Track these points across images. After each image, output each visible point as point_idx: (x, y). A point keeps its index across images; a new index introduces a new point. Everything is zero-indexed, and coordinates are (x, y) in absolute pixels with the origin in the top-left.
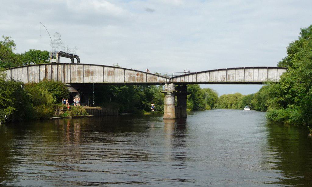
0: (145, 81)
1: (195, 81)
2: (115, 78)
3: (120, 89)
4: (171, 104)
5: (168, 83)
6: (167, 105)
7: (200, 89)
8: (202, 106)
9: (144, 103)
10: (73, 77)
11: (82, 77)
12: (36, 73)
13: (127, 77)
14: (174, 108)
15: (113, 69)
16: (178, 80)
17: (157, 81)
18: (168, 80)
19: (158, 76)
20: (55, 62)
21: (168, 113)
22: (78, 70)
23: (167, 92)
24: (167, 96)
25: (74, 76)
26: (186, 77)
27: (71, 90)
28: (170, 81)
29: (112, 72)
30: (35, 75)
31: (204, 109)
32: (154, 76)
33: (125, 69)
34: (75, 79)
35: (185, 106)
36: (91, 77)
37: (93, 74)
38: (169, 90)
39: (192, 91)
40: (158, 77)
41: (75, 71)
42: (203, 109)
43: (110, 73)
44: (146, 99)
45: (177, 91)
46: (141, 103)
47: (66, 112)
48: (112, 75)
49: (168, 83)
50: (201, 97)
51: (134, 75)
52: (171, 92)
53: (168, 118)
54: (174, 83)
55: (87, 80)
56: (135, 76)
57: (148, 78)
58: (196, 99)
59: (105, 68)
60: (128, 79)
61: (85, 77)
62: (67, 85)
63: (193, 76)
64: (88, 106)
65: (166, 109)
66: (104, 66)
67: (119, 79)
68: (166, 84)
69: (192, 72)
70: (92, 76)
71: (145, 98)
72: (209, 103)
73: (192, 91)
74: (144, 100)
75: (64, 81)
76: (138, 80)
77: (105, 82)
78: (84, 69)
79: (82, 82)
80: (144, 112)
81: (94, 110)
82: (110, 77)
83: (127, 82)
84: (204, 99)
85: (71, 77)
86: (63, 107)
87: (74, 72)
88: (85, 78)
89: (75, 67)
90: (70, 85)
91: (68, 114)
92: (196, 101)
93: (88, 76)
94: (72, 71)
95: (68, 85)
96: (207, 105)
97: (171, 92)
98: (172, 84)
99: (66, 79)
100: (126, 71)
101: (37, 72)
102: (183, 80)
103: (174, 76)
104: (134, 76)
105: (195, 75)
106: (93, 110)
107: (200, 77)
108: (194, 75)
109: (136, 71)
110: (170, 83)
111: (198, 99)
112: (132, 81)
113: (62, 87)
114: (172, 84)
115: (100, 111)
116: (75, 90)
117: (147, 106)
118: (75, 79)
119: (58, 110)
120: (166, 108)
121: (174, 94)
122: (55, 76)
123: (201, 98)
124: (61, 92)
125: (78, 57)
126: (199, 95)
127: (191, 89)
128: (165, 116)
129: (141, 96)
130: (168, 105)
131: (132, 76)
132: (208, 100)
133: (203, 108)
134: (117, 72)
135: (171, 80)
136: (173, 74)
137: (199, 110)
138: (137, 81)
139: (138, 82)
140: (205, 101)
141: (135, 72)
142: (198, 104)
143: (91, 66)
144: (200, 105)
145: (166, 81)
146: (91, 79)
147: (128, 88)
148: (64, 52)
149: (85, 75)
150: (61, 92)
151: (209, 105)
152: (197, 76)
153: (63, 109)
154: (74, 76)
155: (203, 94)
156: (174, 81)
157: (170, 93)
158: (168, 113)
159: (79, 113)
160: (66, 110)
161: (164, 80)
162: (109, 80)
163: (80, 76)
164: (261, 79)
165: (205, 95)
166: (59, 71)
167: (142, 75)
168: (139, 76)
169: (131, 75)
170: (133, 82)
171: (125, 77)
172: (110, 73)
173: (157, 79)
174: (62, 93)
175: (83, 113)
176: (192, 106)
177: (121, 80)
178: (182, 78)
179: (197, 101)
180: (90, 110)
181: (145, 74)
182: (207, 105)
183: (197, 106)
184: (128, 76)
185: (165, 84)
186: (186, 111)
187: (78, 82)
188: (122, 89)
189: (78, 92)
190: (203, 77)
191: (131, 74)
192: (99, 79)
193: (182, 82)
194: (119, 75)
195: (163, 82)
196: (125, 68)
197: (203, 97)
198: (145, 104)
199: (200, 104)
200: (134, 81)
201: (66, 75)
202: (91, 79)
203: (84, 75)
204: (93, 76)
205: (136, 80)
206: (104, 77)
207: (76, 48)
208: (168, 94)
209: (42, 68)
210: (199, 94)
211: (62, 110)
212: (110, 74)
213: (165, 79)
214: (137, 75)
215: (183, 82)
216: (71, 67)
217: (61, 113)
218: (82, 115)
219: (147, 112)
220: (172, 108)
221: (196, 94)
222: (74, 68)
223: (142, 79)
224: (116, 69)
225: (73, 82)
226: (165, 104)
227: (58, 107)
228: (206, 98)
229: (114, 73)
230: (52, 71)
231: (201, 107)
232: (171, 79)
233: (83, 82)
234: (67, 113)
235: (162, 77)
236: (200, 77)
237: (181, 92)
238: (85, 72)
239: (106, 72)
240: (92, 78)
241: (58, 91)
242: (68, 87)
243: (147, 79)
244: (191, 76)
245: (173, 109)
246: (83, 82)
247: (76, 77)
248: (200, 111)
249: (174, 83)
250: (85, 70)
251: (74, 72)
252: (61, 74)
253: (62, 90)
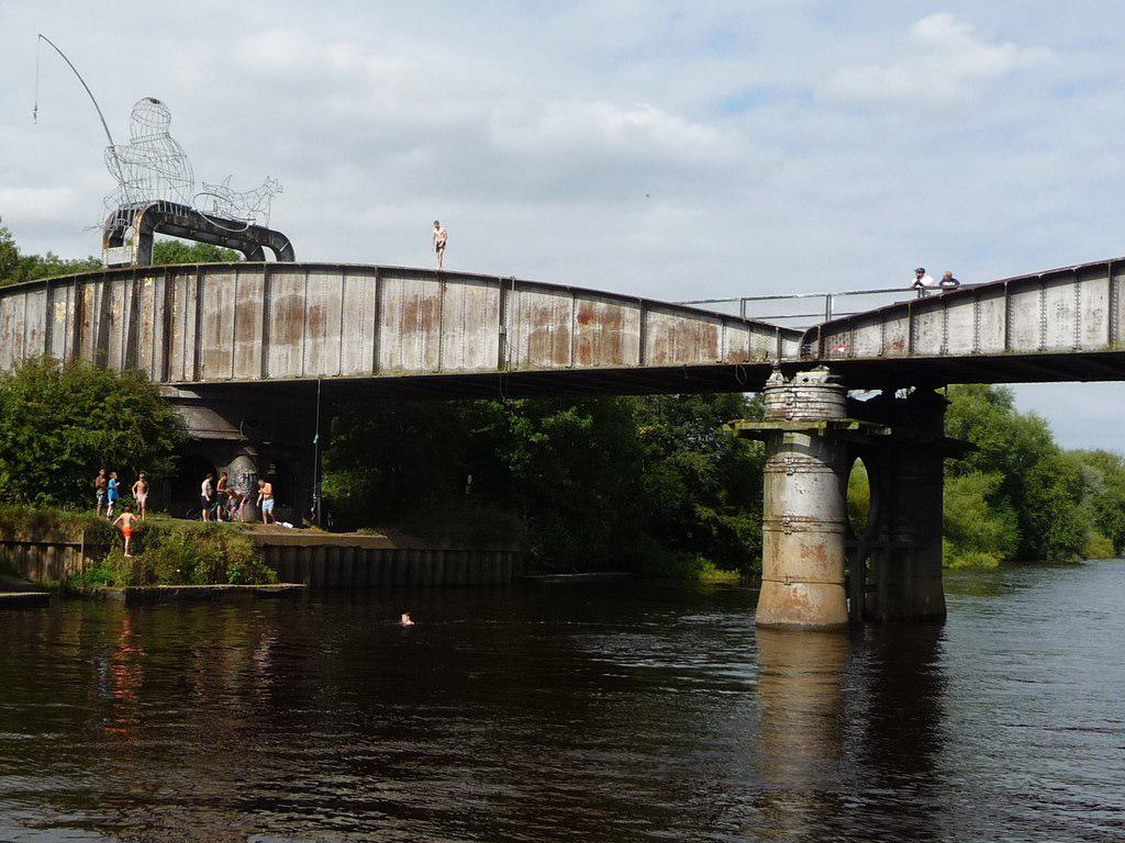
0: (631, 360)
1: (993, 344)
2: (447, 344)
3: (538, 428)
4: (809, 520)
5: (789, 370)
6: (784, 525)
7: (1055, 451)
8: (1066, 538)
9: (705, 512)
10: (213, 348)
11: (258, 342)
12: (33, 333)
13: (520, 335)
14: (834, 550)
15: (431, 288)
16: (869, 343)
17: (713, 355)
18: (792, 349)
19: (726, 320)
20: (125, 264)
21: (789, 581)
22: (242, 301)
23: (780, 433)
24: (785, 456)
25: (218, 342)
26: (922, 318)
27: (196, 423)
28: (804, 352)
29: (427, 304)
30: (29, 341)
31: (1076, 558)
32: (696, 324)
33: (506, 285)
34: (223, 358)
35: (933, 526)
36: (309, 341)
37: (321, 328)
38: (798, 412)
39: (1011, 458)
40: (719, 328)
41: (227, 308)
42: (1071, 554)
43: (419, 317)
44: (722, 495)
45: (855, 426)
46: (691, 513)
47: (108, 560)
48: (426, 324)
49: (789, 370)
50: (1058, 489)
51: (563, 319)
52: (811, 432)
53: (785, 621)
54: (835, 367)
55: (284, 364)
56: (569, 325)
57: (651, 339)
58: (1030, 501)
59: (393, 286)
60: (524, 352)
61: (279, 342)
62: (176, 393)
63: (977, 311)
64: (314, 523)
65: (776, 553)
66: (383, 273)
67: (472, 352)
68: (775, 378)
69: (969, 278)
70: (315, 335)
71: (715, 490)
72: (1103, 525)
73: (1011, 458)
74: (710, 501)
75: (167, 369)
76: (585, 350)
77: (388, 369)
78: (274, 299)
79: (255, 377)
80: (701, 568)
81: (336, 553)
82: (418, 343)
83: (520, 369)
84: (1077, 500)
85: (204, 346)
86: (81, 527)
87: (219, 317)
88: (275, 351)
89: (225, 285)
90: (195, 396)
91: (119, 569)
92: (1034, 515)
93: (292, 337)
94: (209, 309)
95: (183, 394)
96: (1094, 536)
97: (811, 432)
98: (819, 375)
99: (177, 360)
100: (515, 298)
101: (39, 326)
102: (899, 345)
103: (834, 318)
104: (562, 329)
105: (998, 304)
106: (328, 549)
107: (1036, 311)
108: (984, 305)
109: (576, 293)
110: (807, 367)
111: (1043, 502)
112: (547, 363)
113: (129, 403)
114: (819, 375)
115: (377, 557)
116: (224, 425)
117: (727, 532)
118: (223, 358)
119: (60, 547)
120: (776, 545)
121: (834, 446)
122: (150, 354)
123: (1058, 497)
124: (115, 435)
125: (286, 240)
126: (1047, 482)
127: (1005, 452)
128: (769, 606)
129: (689, 476)
130: (787, 525)
131: (552, 327)
132: (1100, 509)
133: (1073, 550)
134: (459, 303)
135: (815, 347)
136: (828, 304)
137: (1049, 557)
138: (583, 360)
139: (591, 366)
140: (1083, 513)
141: (571, 300)
142: (1046, 527)
143: (313, 277)
144: (1056, 535)
145: (780, 354)
146: (307, 358)
147: (587, 422)
148: (186, 210)
149: (279, 330)
150: (115, 435)
151: (1107, 535)
152: (1016, 309)
153: (81, 540)
154: (218, 342)
155: (1071, 478)
156: (839, 349)
157: (803, 440)
158: (789, 581)
159: (201, 569)
160: (107, 549)
161: (761, 347)
162: (408, 357)
163: (249, 337)
164: (954, 590)
165: (1081, 481)
166: (143, 317)
167: (616, 319)
168: (598, 327)
169: (541, 323)
170: (556, 366)
171: (502, 336)
172: (419, 317)
173: (712, 344)
174: (121, 440)
175: (232, 571)
176: (1011, 537)
177: (483, 360)
178: (898, 329)
179: (1037, 510)
180: (299, 548)
181: (631, 314)
182: (1094, 536)
183: (1039, 542)
184: (528, 329)
185: (773, 376)
186: (936, 571)
187: (239, 377)
188: (550, 431)
189: (242, 437)
190: (1062, 311)
191: (544, 315)
192: (352, 356)
193: (892, 353)
194: (470, 323)
195: (759, 360)
196: (508, 276)
197: (1070, 489)
198: (715, 521)
199: (1056, 527)
200: (562, 359)
201: (178, 335)
202: (307, 358)
203: (273, 334)
204: (320, 340)
205: (578, 358)
206: (383, 337)
207: (271, 189)
208: (792, 447)
209: (64, 304)
210: (1052, 474)
211: (77, 548)
212: (423, 318)
213: (772, 343)
214: (584, 318)
215: (904, 354)
216: (206, 290)
217: (75, 562)
218: (227, 582)
219: (718, 568)
220: (821, 547)
221: (1032, 476)
222: (219, 292)
223: (616, 344)
224: (455, 289)
225: (210, 375)
226: (767, 516)
227: (57, 526)
228: (1088, 499)
229: (440, 317)
230: (107, 317)
231: (1062, 546)
232: (811, 335)
233: (264, 373)
234: (113, 569)
235: (753, 326)
236: (1036, 311)
237: (888, 431)
238: (280, 316)
239: (391, 308)
240: (315, 346)
241: (101, 427)
242: (182, 411)
243: (663, 344)
244: (963, 314)
245: (828, 552)
246: (264, 373)
247: (227, 346)
248: (1059, 563)
249: (835, 367)
250: (280, 306)
251: (219, 317)
252: (151, 330)
253: (127, 424)
